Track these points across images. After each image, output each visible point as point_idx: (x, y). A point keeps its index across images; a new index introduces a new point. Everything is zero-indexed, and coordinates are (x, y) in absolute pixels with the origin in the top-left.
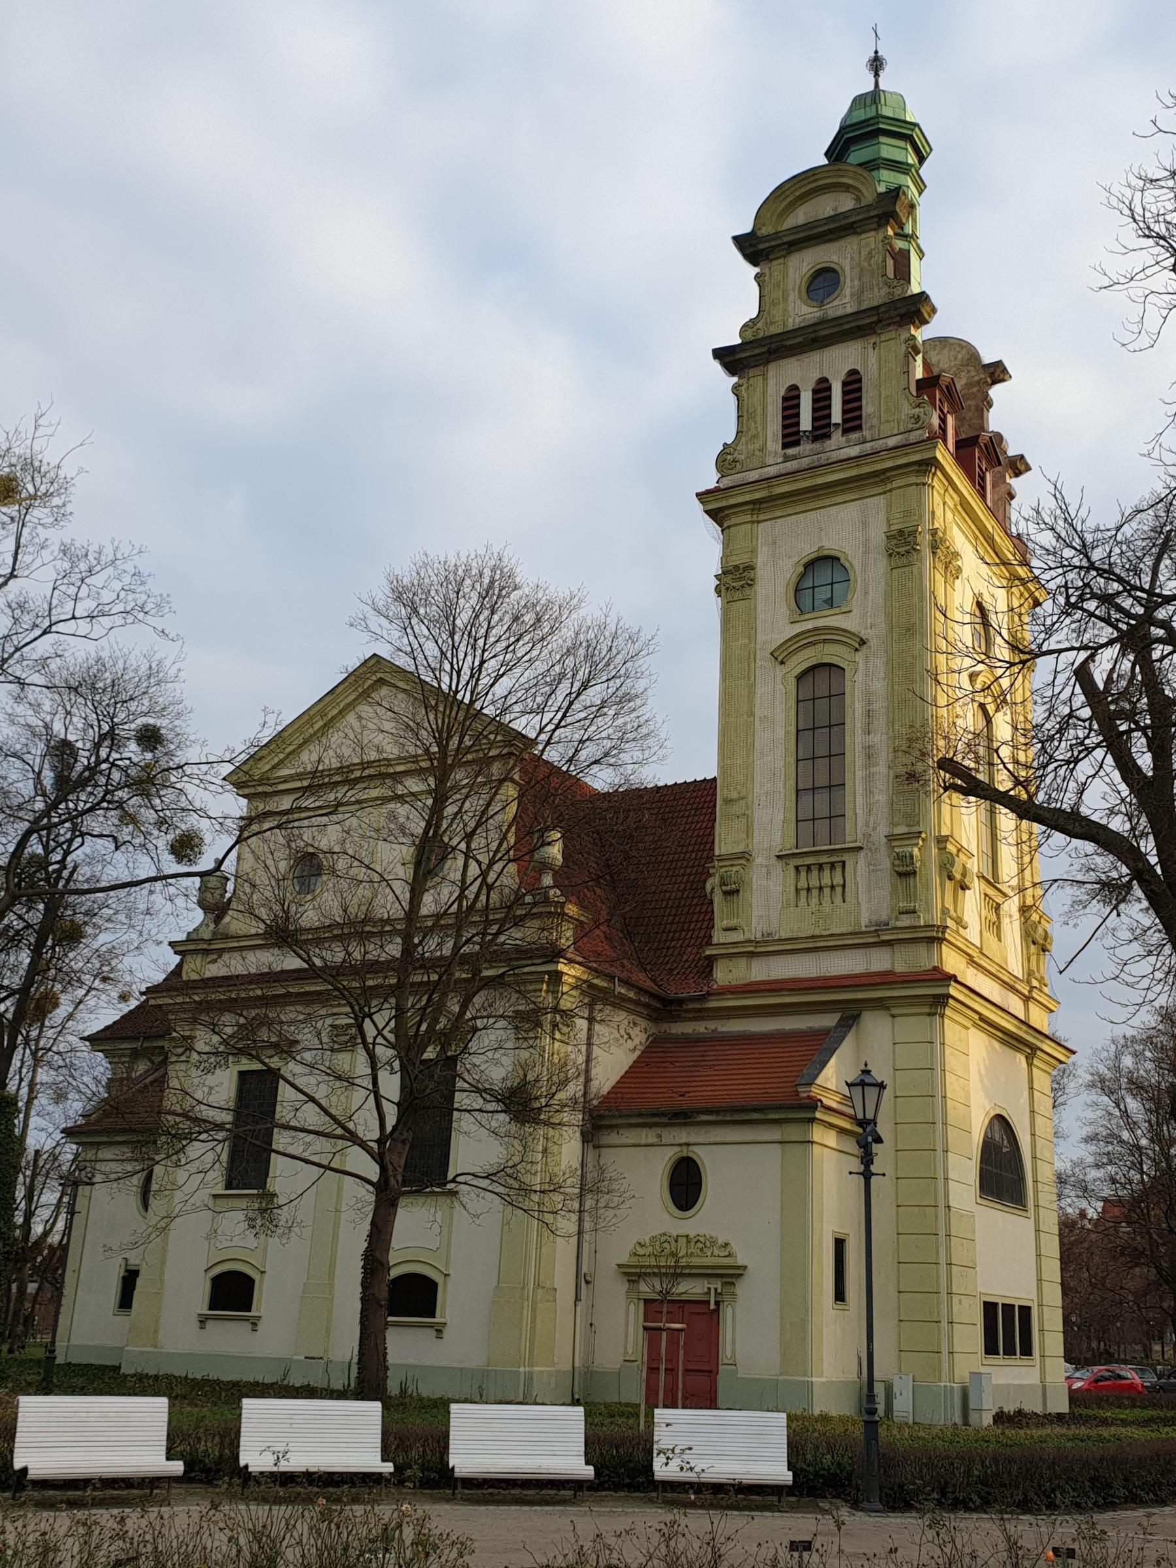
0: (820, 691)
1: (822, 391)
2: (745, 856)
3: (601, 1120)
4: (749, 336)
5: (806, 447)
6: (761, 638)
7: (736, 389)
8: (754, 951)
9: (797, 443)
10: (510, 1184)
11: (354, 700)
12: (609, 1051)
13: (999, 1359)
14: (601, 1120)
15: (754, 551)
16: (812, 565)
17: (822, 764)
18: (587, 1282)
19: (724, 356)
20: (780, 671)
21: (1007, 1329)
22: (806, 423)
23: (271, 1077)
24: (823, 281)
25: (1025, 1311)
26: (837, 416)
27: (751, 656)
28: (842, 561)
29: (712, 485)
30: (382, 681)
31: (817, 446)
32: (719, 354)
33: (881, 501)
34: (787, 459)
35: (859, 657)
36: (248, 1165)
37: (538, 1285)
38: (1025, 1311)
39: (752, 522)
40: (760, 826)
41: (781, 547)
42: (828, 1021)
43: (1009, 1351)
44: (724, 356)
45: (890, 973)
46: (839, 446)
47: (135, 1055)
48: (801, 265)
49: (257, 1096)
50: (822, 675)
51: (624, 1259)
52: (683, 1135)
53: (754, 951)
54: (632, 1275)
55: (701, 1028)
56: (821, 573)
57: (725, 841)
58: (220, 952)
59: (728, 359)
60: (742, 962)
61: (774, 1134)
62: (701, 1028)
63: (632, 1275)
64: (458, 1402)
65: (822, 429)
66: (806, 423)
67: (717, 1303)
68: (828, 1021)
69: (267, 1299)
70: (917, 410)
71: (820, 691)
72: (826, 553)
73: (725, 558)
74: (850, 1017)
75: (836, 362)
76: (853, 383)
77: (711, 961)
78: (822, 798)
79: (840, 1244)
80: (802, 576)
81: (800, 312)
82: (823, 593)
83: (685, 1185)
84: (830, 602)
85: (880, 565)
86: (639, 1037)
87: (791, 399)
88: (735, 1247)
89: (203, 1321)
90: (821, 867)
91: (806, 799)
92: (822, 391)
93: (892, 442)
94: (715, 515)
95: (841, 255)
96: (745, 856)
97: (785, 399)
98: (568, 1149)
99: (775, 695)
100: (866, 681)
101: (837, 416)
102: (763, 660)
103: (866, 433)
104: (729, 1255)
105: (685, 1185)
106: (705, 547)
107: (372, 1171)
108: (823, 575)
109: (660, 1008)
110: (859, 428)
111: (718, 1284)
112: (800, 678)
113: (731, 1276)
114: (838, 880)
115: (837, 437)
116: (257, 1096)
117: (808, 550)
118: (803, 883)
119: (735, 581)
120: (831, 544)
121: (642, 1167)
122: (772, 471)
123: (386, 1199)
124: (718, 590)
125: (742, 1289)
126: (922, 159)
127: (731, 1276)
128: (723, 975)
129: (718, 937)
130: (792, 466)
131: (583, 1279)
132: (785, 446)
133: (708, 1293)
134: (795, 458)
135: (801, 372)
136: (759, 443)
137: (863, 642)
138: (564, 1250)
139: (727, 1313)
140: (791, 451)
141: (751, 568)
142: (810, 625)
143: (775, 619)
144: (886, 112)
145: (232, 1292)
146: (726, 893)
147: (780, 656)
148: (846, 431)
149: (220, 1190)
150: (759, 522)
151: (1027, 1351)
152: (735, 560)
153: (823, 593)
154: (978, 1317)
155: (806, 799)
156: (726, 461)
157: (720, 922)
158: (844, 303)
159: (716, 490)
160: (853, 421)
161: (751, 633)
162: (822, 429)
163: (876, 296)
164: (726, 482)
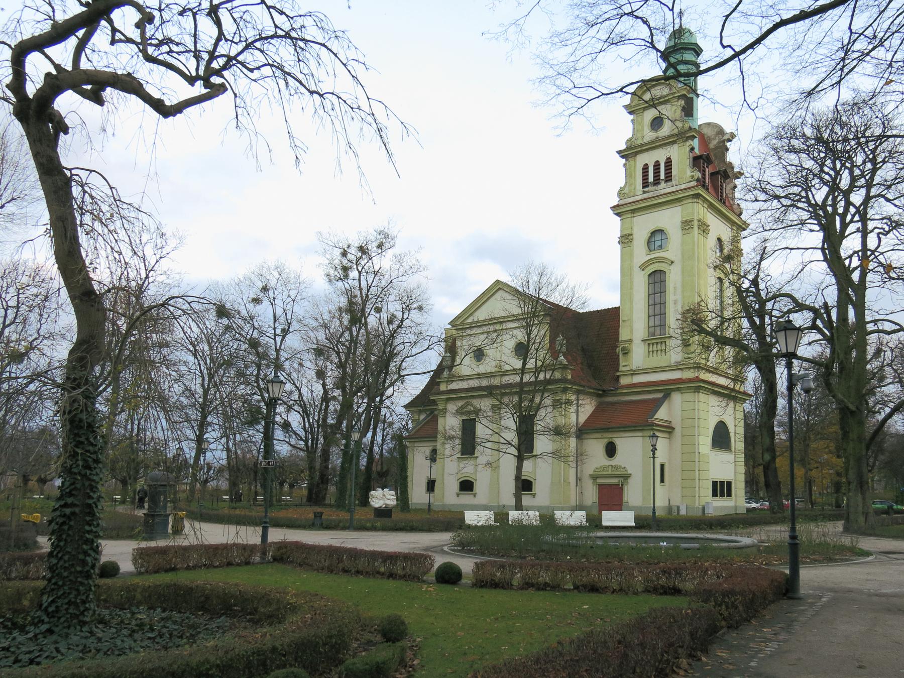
0: (657, 279)
2: (630, 341)
3: (582, 432)
5: (651, 188)
6: (635, 260)
7: (625, 165)
8: (633, 373)
9: (647, 186)
10: (556, 455)
11: (516, 328)
12: (583, 409)
13: (718, 498)
14: (582, 432)
16: (653, 233)
17: (658, 307)
20: (643, 272)
21: (721, 489)
22: (651, 179)
23: (473, 421)
24: (657, 123)
25: (729, 484)
26: (662, 176)
27: (632, 268)
29: (616, 203)
30: (500, 289)
31: (656, 188)
32: (619, 152)
33: (679, 208)
34: (644, 192)
35: (672, 267)
36: (469, 447)
37: (564, 481)
38: (729, 484)
40: (635, 328)
41: (644, 224)
42: (660, 395)
43: (722, 495)
45: (681, 379)
47: (420, 412)
49: (468, 428)
50: (657, 275)
51: (591, 473)
52: (610, 435)
53: (633, 373)
54: (594, 478)
55: (616, 399)
56: (657, 236)
57: (624, 335)
58: (452, 381)
60: (630, 377)
61: (640, 434)
62: (616, 399)
63: (594, 478)
65: (657, 181)
66: (651, 179)
68: (660, 395)
69: (477, 488)
71: (657, 279)
73: (622, 230)
74: (667, 395)
75: (660, 155)
76: (669, 162)
77: (618, 377)
78: (658, 285)
79: (662, 466)
80: (650, 237)
81: (649, 135)
82: (658, 244)
83: (611, 450)
84: (661, 247)
85: (679, 232)
86: (594, 403)
87: (645, 169)
88: (628, 468)
89: (458, 495)
90: (657, 343)
91: (652, 318)
92: (657, 165)
93: (683, 187)
94: (617, 214)
96: (630, 341)
98: (573, 441)
99: (641, 282)
100: (674, 278)
101: (662, 176)
102: (636, 269)
103: (674, 182)
105: (611, 450)
107: (516, 453)
108: (658, 237)
109: (600, 394)
111: (622, 479)
112: (649, 275)
113: (626, 477)
114: (663, 348)
115: (663, 184)
116: (468, 428)
117: (653, 228)
118: (651, 349)
119: (626, 239)
121: (595, 447)
122: (638, 198)
123: (520, 459)
124: (619, 242)
125: (630, 480)
126: (698, 55)
128: (624, 381)
129: (621, 368)
130: (646, 196)
131: (578, 479)
132: (643, 187)
134: (646, 192)
135: (649, 158)
136: (633, 187)
137: (672, 262)
138: (572, 472)
139: (625, 488)
140: (646, 189)
143: (641, 253)
145: (467, 486)
147: (643, 267)
148: (666, 181)
149: (459, 455)
151: (729, 495)
152: (627, 232)
153: (658, 244)
155: (652, 318)
156: (621, 193)
157: (622, 362)
158: (667, 129)
160: (669, 178)
161: (632, 259)
162: (657, 181)
164: (622, 202)
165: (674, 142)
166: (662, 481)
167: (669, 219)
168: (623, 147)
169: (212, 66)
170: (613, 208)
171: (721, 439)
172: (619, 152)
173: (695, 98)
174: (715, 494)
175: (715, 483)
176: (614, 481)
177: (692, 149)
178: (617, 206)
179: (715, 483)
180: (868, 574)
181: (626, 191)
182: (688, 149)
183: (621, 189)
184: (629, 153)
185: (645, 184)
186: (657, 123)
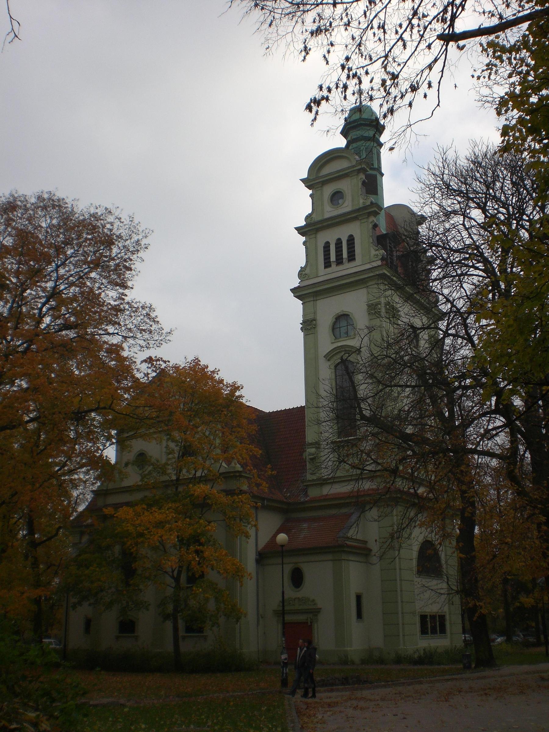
1: (339, 243)
4: (309, 220)
8: (323, 482)
15: (315, 313)
18: (262, 617)
19: (300, 230)
21: (432, 624)
22: (333, 258)
24: (337, 196)
28: (351, 316)
29: (297, 285)
32: (297, 229)
33: (364, 291)
39: (314, 300)
41: (328, 308)
43: (434, 631)
44: (300, 230)
46: (348, 268)
48: (328, 190)
53: (323, 482)
56: (342, 320)
59: (301, 231)
61: (330, 557)
64: (379, 266)
65: (339, 261)
66: (333, 258)
67: (311, 623)
70: (377, 252)
72: (345, 313)
73: (304, 316)
75: (343, 232)
76: (351, 240)
79: (359, 598)
80: (335, 323)
81: (329, 211)
92: (339, 243)
93: (368, 266)
94: (298, 297)
95: (345, 186)
97: (324, 247)
104: (315, 604)
105: (297, 578)
106: (296, 308)
108: (343, 323)
110: (354, 259)
113: (316, 612)
115: (334, 267)
119: (309, 326)
120: (346, 309)
124: (302, 329)
127: (316, 612)
133: (307, 620)
135: (330, 236)
141: (315, 320)
142: (340, 344)
143: (326, 343)
144: (365, 116)
146: (311, 459)
147: (329, 357)
150: (316, 300)
153: (343, 330)
154: (417, 619)
156: (302, 274)
158: (347, 206)
159: (299, 287)
160: (352, 257)
162: (339, 261)
163: (361, 202)
165: (356, 218)
166: (359, 615)
167: (355, 303)
168: (303, 223)
169: (466, 515)
170: (293, 290)
171: (428, 563)
172: (297, 229)
173: (378, 176)
174: (424, 631)
175: (423, 618)
176: (301, 618)
177: (375, 226)
178: (298, 287)
179: (423, 618)
180: (330, 698)
181: (307, 271)
182: (371, 226)
183: (302, 270)
184: (309, 229)
185: (328, 264)
186: (337, 196)
